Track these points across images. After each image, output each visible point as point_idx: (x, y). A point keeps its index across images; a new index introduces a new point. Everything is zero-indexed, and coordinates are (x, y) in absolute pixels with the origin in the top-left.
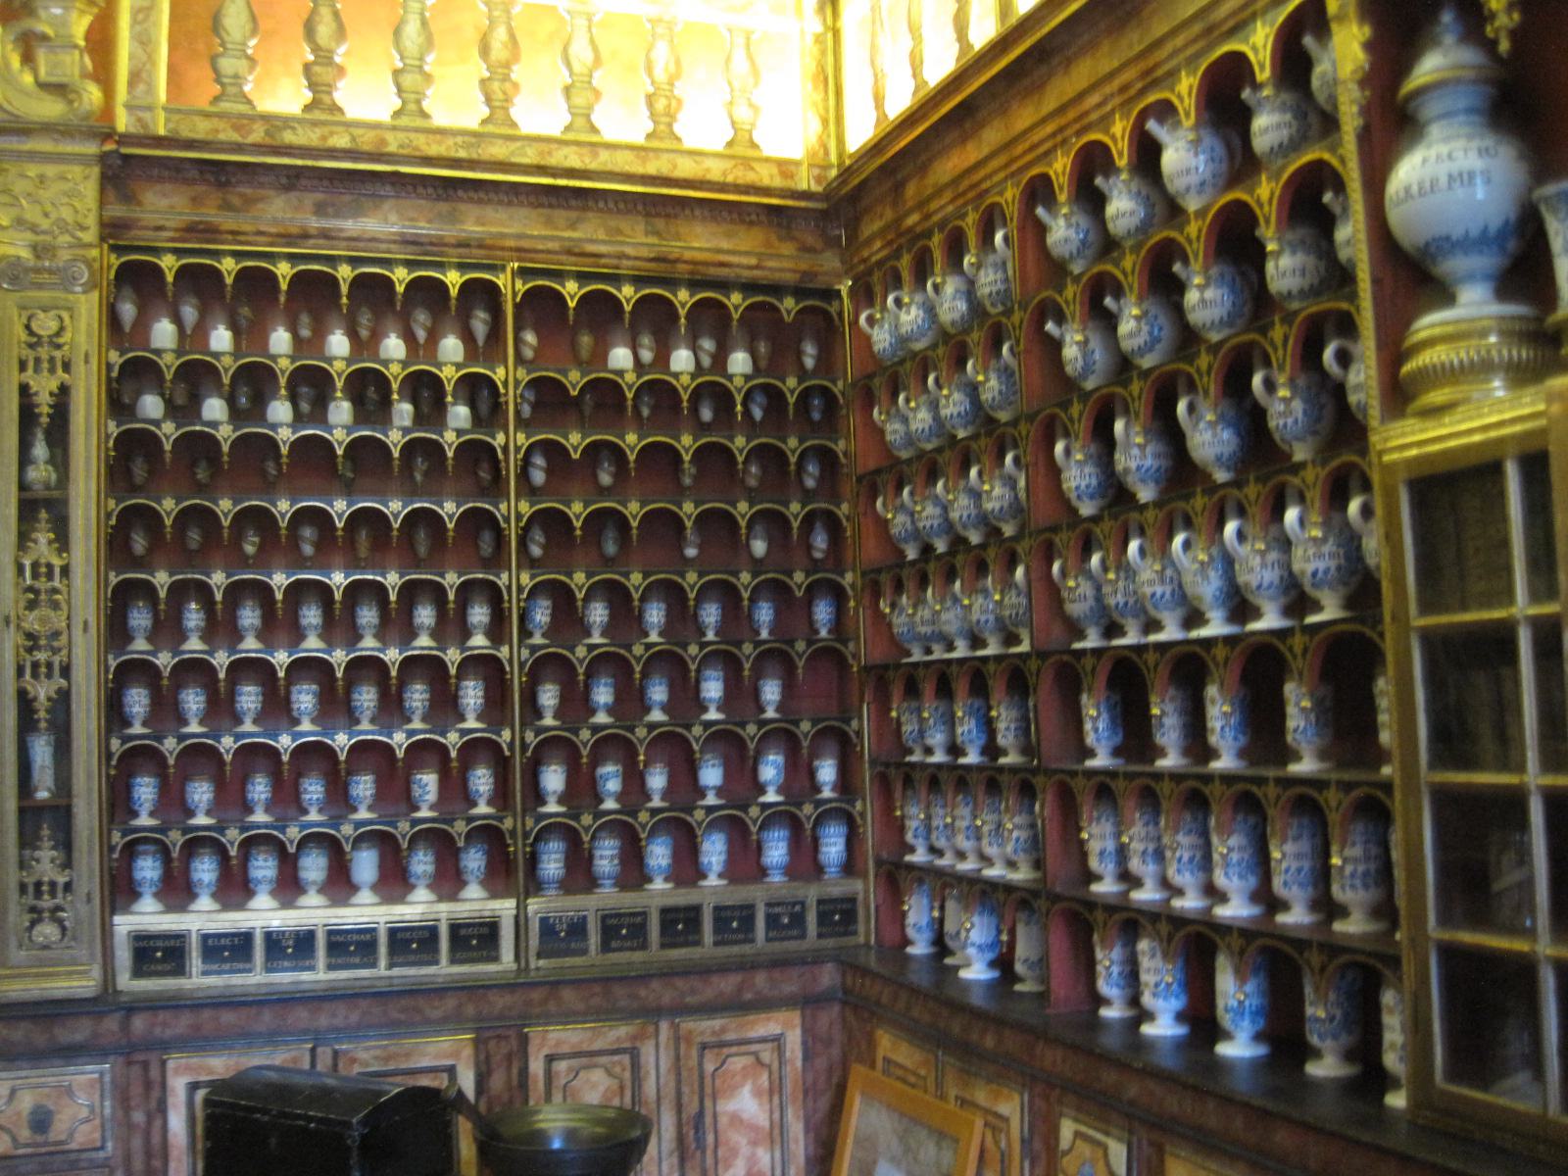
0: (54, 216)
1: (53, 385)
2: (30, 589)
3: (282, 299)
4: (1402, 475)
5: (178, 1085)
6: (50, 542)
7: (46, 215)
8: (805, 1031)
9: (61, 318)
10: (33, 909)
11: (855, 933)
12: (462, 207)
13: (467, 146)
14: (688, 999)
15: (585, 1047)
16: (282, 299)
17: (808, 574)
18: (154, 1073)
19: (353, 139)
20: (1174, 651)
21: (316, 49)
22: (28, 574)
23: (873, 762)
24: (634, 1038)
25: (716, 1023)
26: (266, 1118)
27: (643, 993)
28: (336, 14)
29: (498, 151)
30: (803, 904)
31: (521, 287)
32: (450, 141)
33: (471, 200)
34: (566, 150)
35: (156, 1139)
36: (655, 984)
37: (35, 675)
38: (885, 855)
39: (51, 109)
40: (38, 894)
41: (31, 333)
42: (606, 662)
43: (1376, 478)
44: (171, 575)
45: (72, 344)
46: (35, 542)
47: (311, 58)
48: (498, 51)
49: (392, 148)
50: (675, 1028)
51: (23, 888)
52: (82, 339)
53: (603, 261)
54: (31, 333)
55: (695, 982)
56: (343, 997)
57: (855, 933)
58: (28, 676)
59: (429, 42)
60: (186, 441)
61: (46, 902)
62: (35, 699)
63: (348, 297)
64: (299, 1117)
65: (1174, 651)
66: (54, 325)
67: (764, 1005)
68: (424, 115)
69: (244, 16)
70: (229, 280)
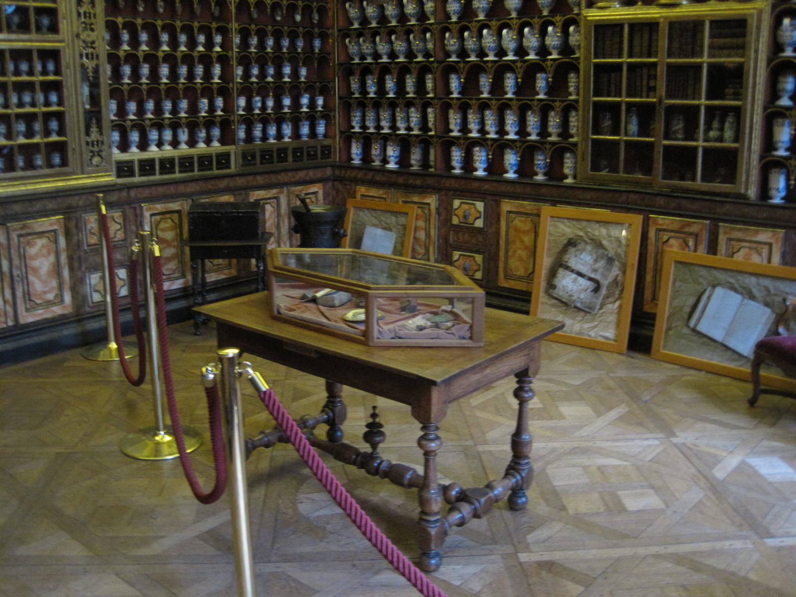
2: (84, 23)
4: (593, 24)
14: (292, 180)
15: (265, 197)
18: (138, 212)
20: (400, 65)
22: (82, 17)
23: (340, 98)
24: (278, 193)
25: (300, 188)
27: (279, 177)
36: (283, 174)
38: (343, 130)
43: (582, 24)
44: (123, 18)
62: (88, 68)
64: (235, 212)
65: (400, 65)
67: (312, 182)
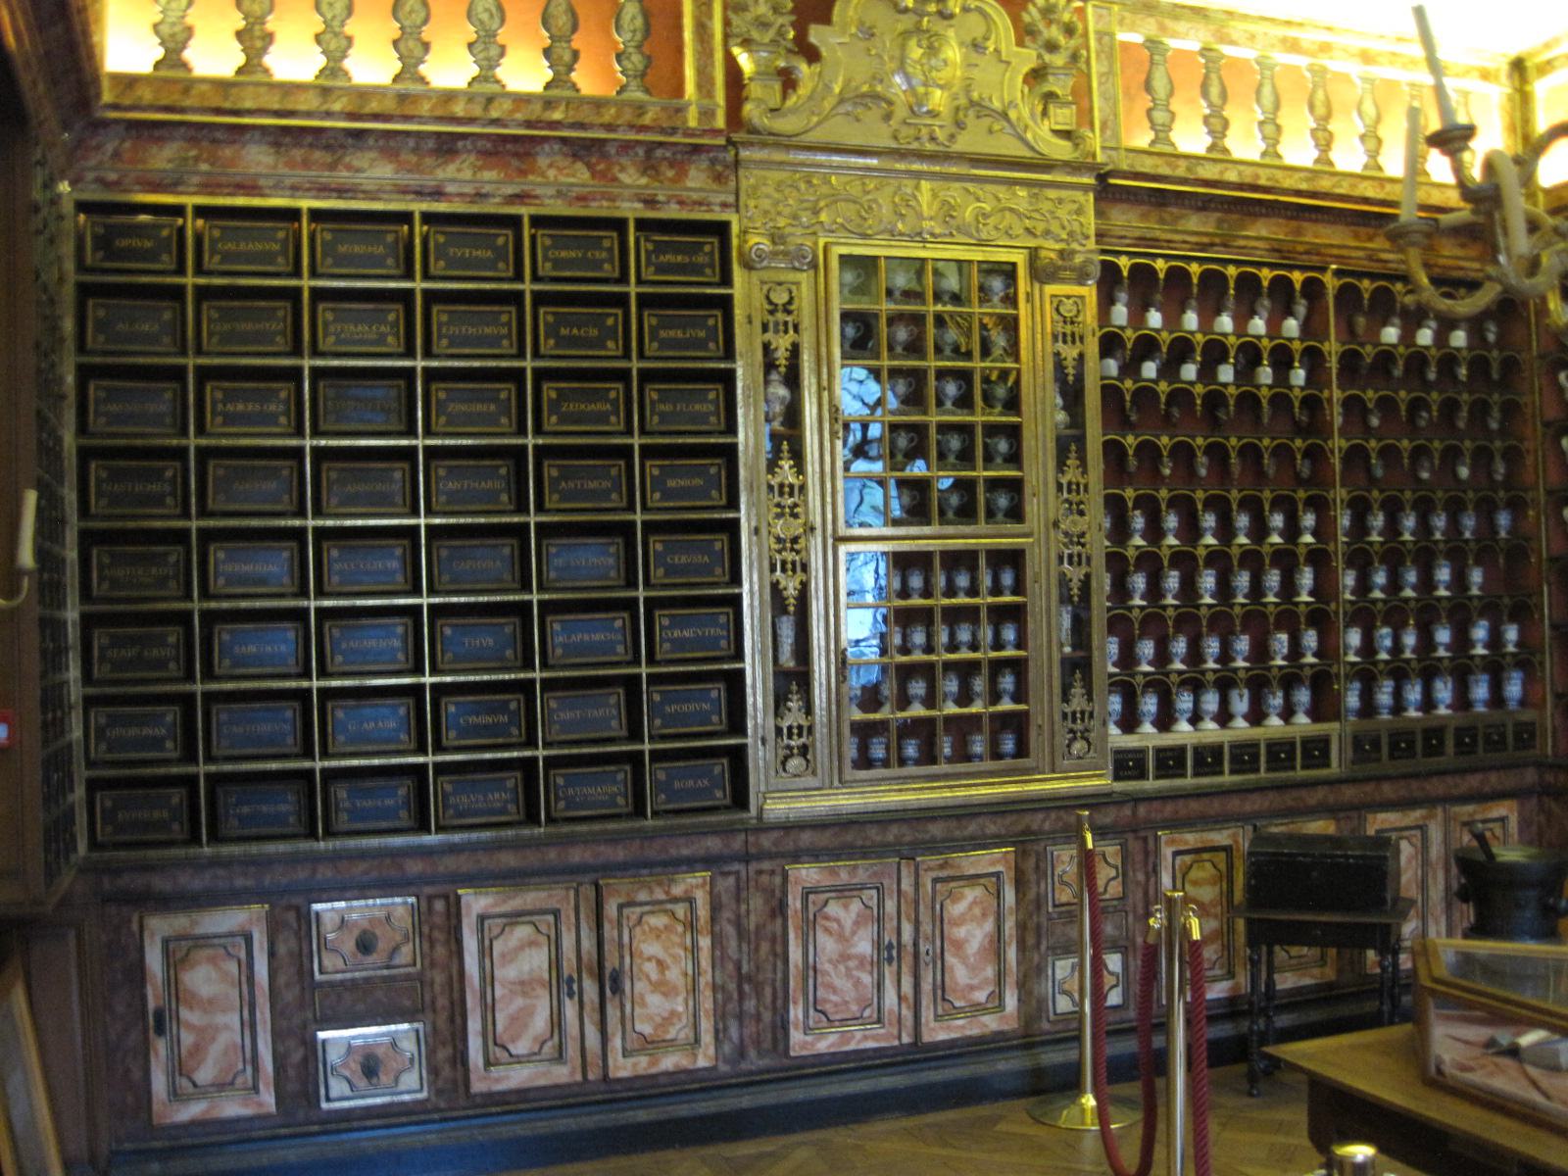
0: (1068, 229)
1: (1075, 353)
3: (1195, 290)
5: (1167, 852)
6: (791, 467)
7: (1064, 228)
8: (1520, 814)
9: (790, 292)
10: (1071, 731)
11: (1534, 747)
12: (1305, 224)
13: (1307, 180)
16: (1195, 290)
17: (1414, 491)
19: (1240, 173)
21: (1210, 105)
24: (1425, 818)
25: (1470, 808)
26: (1309, 860)
28: (1220, 78)
29: (1325, 184)
30: (1503, 725)
31: (1338, 283)
32: (1297, 175)
33: (1310, 220)
34: (1366, 184)
35: (1151, 891)
36: (1435, 780)
37: (784, 570)
39: (1062, 150)
40: (1074, 721)
41: (770, 302)
42: (1180, 559)
45: (1084, 322)
46: (781, 468)
47: (1207, 111)
48: (1321, 110)
49: (1263, 182)
50: (1445, 811)
51: (1065, 716)
52: (1089, 320)
53: (1353, 262)
54: (770, 302)
55: (1458, 779)
56: (1181, 796)
57: (1534, 747)
58: (778, 573)
59: (1171, 94)
60: (1173, 396)
61: (1079, 726)
63: (1235, 289)
66: (785, 298)
68: (1278, 156)
69: (1165, 80)
70: (1162, 276)
